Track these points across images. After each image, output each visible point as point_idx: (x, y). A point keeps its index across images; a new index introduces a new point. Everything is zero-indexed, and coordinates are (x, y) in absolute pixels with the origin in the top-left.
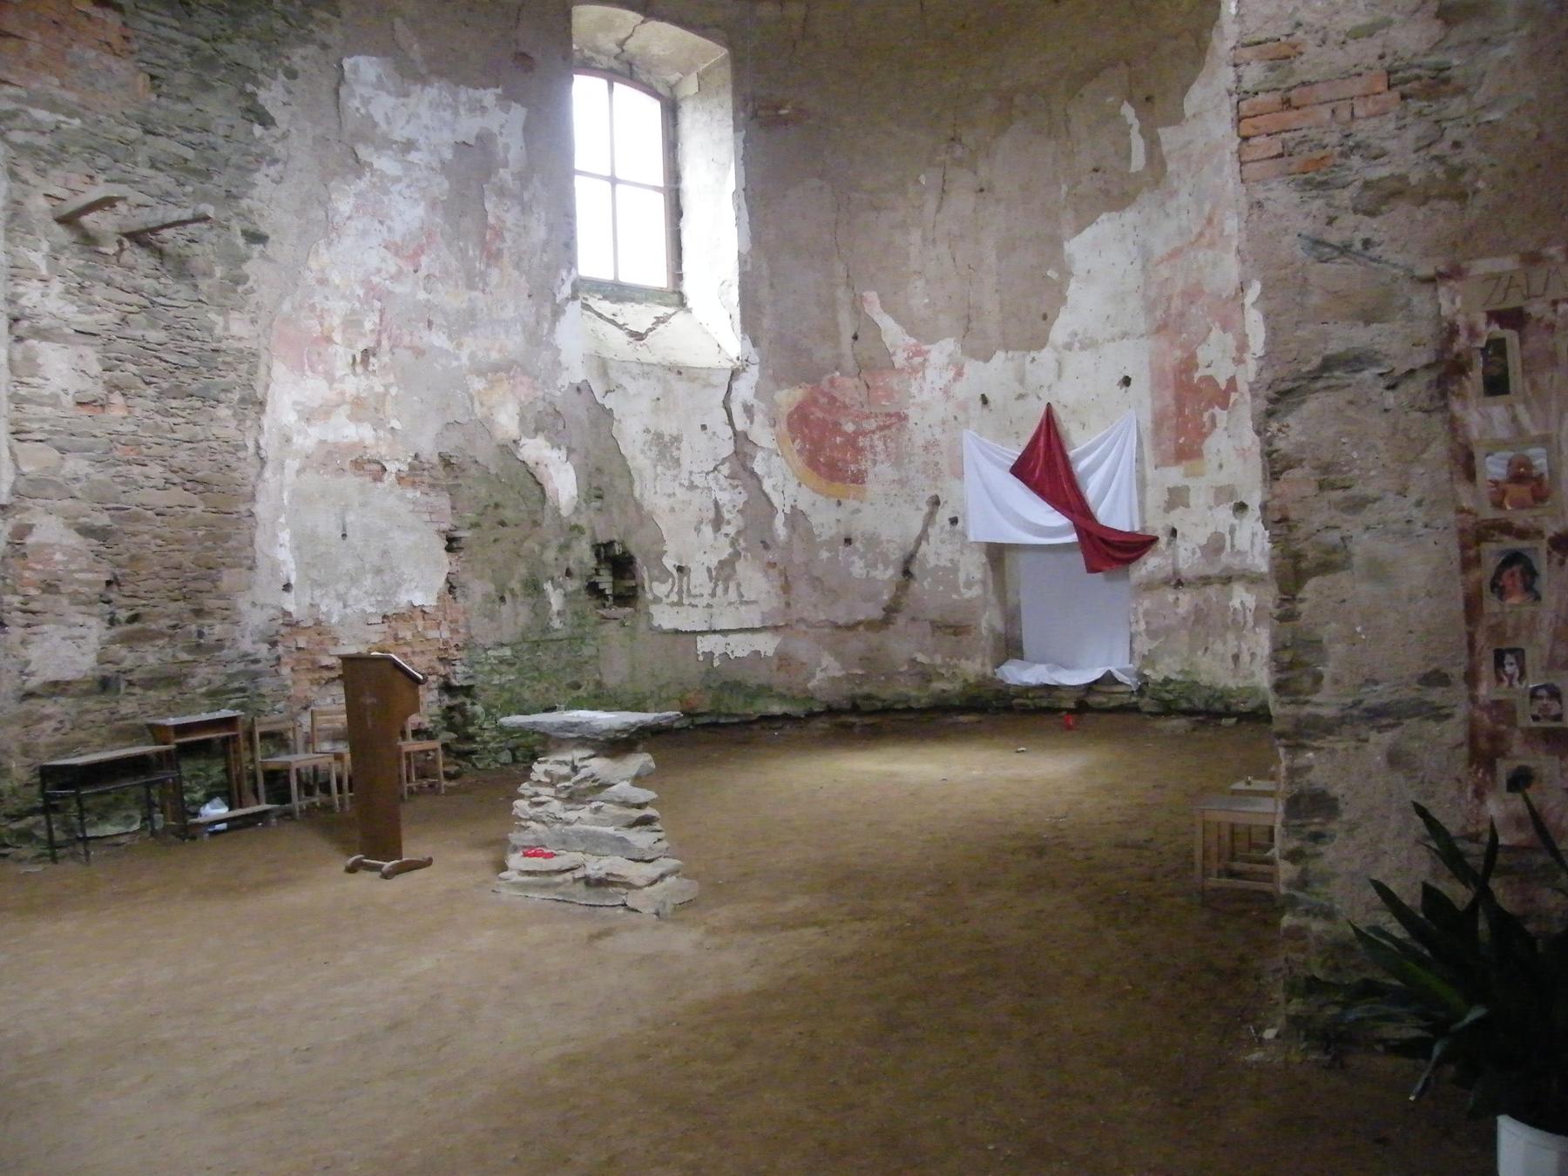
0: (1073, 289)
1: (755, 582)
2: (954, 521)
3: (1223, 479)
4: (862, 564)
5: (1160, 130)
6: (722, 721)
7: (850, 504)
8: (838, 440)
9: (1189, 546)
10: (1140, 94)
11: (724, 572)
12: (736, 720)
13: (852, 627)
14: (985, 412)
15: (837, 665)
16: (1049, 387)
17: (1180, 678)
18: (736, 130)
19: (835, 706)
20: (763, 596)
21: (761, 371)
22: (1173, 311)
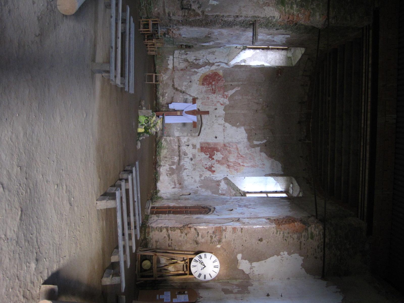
0: (234, 128)
3: (197, 156)
5: (260, 147)
8: (211, 81)
11: (186, 60)
14: (213, 109)
15: (166, 79)
16: (217, 122)
17: (162, 146)
18: (277, 66)
19: (157, 78)
20: (180, 66)
21: (227, 68)
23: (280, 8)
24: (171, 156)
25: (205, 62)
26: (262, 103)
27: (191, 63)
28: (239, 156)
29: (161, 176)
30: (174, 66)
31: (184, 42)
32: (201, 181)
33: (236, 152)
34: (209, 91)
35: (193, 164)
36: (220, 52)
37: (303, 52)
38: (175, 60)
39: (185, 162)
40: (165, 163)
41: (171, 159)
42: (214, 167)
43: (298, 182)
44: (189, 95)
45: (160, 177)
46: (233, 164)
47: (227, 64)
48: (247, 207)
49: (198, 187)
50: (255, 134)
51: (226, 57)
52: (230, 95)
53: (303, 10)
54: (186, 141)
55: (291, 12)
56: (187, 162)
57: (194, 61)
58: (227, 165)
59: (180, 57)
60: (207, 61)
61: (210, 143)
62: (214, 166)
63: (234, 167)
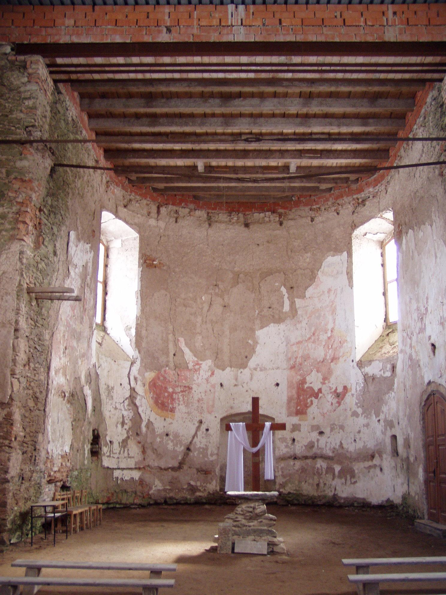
0: (258, 349)
1: (134, 449)
3: (315, 423)
6: (118, 506)
7: (169, 420)
8: (166, 394)
9: (301, 445)
11: (124, 444)
13: (166, 469)
14: (222, 389)
15: (160, 485)
16: (247, 383)
17: (295, 492)
19: (159, 501)
20: (136, 455)
23: (2, 240)
24: (314, 474)
25: (129, 405)
26: (210, 296)
28: (313, 338)
29: (357, 496)
30: (136, 468)
31: (83, 446)
32: (366, 413)
33: (306, 344)
34: (186, 398)
36: (108, 376)
37: (112, 216)
38: (122, 466)
39: (326, 445)
40: (330, 487)
41: (321, 474)
43: (363, 223)
44: (193, 437)
45: (358, 498)
46: (330, 351)
47: (132, 364)
48: (426, 314)
49: (378, 419)
50: (271, 309)
52: (194, 358)
53: (10, 194)
54: (285, 444)
55: (12, 218)
56: (327, 443)
57: (126, 427)
58: (332, 362)
59: (116, 456)
60: (127, 402)
61: (288, 397)
63: (336, 348)
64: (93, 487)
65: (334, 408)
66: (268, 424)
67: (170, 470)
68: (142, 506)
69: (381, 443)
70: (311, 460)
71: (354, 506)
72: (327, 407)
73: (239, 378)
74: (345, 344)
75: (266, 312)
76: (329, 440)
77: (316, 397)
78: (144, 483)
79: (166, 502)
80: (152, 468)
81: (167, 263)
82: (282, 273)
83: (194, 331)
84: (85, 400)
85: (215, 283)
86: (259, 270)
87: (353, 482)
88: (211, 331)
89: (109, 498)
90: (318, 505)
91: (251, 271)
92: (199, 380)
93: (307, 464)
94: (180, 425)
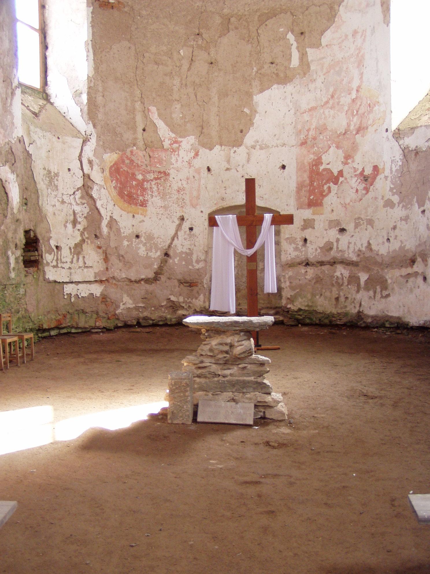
0: (257, 119)
1: (92, 256)
2: (191, 229)
3: (334, 217)
4: (144, 249)
6: (73, 331)
7: (139, 217)
8: (134, 183)
9: (314, 247)
10: (297, 30)
12: (80, 331)
14: (209, 175)
15: (131, 302)
16: (243, 166)
17: (307, 308)
19: (129, 323)
20: (96, 264)
21: (97, 141)
22: (310, 136)
24: (333, 285)
25: (82, 197)
26: (191, 50)
27: (87, 235)
28: (331, 102)
29: (390, 314)
30: (96, 281)
34: (161, 188)
35: (356, 227)
36: (48, 157)
39: (348, 247)
40: (353, 302)
41: (342, 285)
42: (363, 169)
44: (173, 239)
45: (391, 317)
46: (355, 119)
47: (85, 142)
49: (422, 209)
50: (274, 65)
51: (64, 143)
52: (171, 133)
54: (293, 245)
56: (349, 243)
57: (79, 227)
59: (67, 266)
60: (78, 194)
62: (360, 170)
63: (364, 114)
64: (30, 308)
65: (360, 197)
66: (268, 217)
67: (142, 282)
68: (107, 330)
69: (425, 242)
70: (328, 266)
71: (385, 327)
72: (351, 195)
73: (231, 159)
74: (376, 108)
75: (267, 69)
76: (353, 240)
77: (335, 180)
78: (108, 300)
79: (139, 324)
80: (119, 281)
81: (130, 3)
82: (289, 13)
83: (170, 97)
84: (4, 187)
85: (197, 32)
86: (256, 11)
87: (384, 295)
88: (193, 97)
89: (59, 321)
90: (337, 326)
91: (246, 13)
92: (178, 163)
93: (323, 272)
94: (154, 224)
